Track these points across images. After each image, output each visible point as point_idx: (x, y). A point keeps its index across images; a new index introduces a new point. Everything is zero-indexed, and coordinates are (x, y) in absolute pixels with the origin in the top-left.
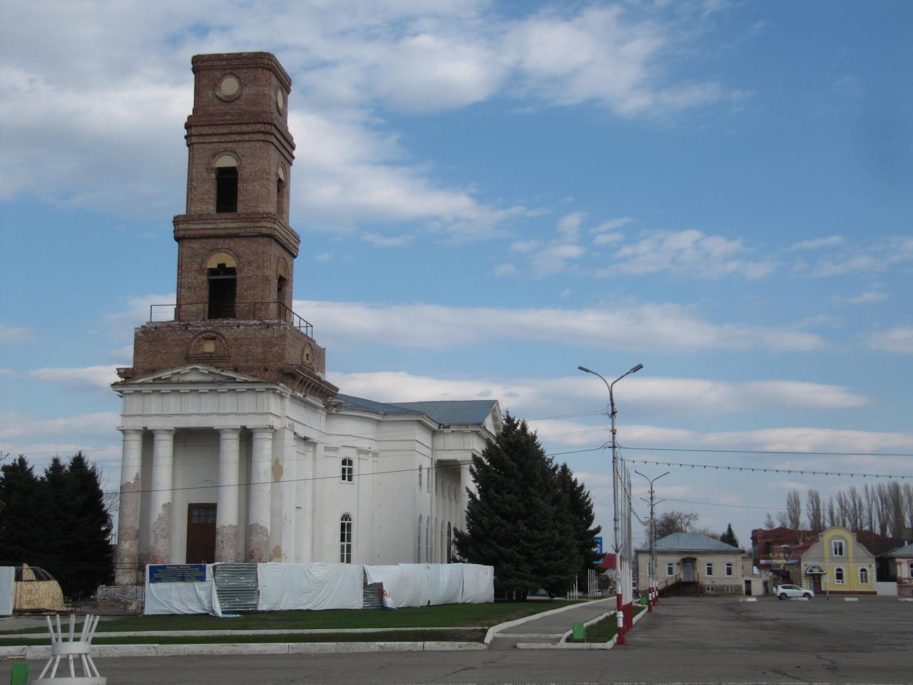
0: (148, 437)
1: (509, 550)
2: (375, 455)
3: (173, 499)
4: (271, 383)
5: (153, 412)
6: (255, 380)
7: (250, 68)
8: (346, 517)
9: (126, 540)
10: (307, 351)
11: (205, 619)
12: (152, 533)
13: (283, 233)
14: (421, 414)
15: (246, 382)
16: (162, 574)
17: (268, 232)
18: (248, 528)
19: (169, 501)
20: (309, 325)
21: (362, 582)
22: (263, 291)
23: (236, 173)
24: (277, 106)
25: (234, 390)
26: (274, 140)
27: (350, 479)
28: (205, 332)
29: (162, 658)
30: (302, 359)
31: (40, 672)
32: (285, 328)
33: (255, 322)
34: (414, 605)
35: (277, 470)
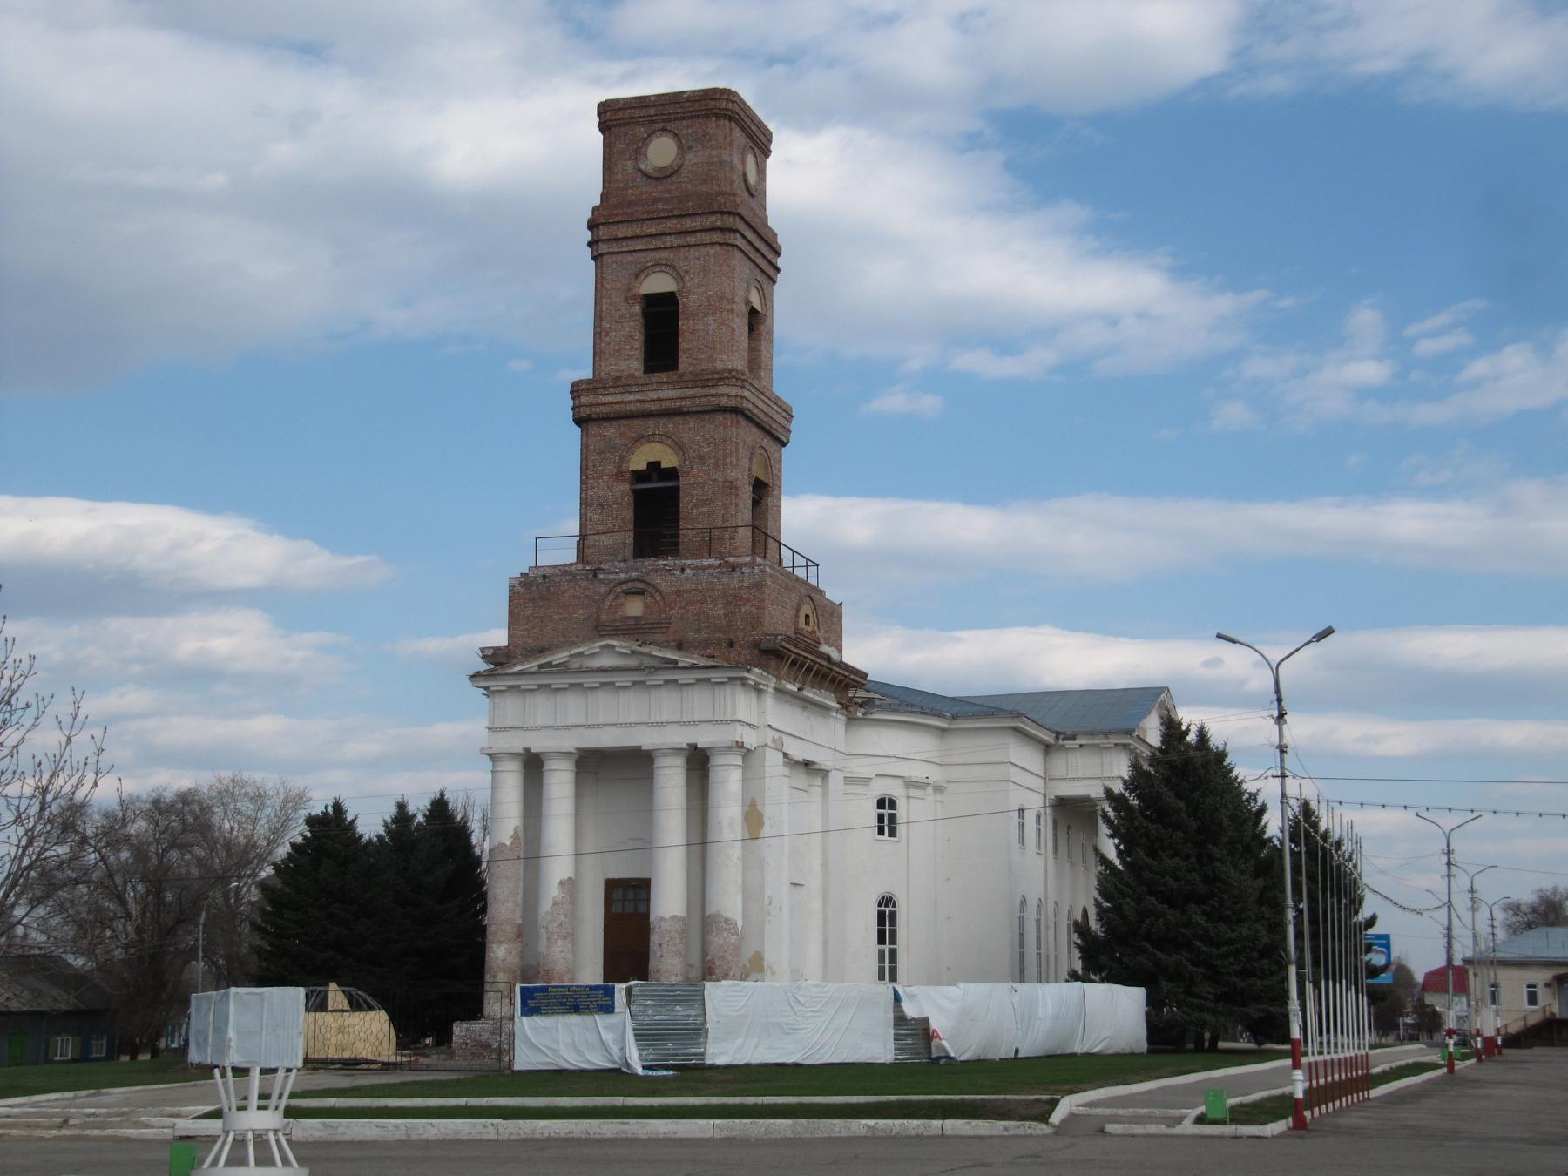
0: (533, 765)
1: (1175, 958)
2: (939, 789)
3: (577, 870)
4: (736, 667)
5: (540, 723)
6: (711, 662)
7: (697, 117)
8: (887, 901)
9: (501, 943)
10: (807, 609)
11: (614, 1078)
12: (543, 931)
13: (760, 404)
14: (1018, 715)
15: (694, 667)
16: (543, 998)
17: (733, 404)
18: (704, 921)
19: (572, 875)
20: (810, 563)
21: (891, 1015)
22: (724, 506)
23: (676, 303)
24: (746, 181)
25: (676, 681)
26: (740, 242)
27: (893, 833)
28: (626, 582)
29: (508, 1142)
30: (797, 623)
31: (202, 1161)
32: (763, 571)
33: (712, 561)
34: (989, 1057)
35: (753, 819)
